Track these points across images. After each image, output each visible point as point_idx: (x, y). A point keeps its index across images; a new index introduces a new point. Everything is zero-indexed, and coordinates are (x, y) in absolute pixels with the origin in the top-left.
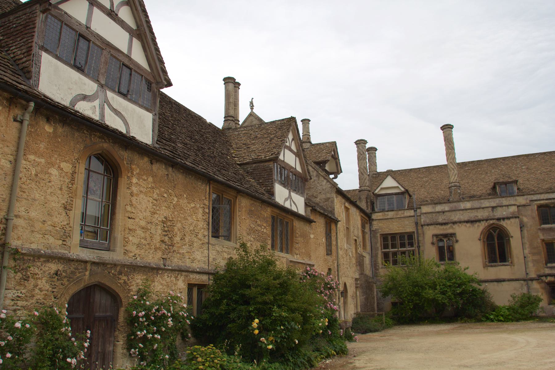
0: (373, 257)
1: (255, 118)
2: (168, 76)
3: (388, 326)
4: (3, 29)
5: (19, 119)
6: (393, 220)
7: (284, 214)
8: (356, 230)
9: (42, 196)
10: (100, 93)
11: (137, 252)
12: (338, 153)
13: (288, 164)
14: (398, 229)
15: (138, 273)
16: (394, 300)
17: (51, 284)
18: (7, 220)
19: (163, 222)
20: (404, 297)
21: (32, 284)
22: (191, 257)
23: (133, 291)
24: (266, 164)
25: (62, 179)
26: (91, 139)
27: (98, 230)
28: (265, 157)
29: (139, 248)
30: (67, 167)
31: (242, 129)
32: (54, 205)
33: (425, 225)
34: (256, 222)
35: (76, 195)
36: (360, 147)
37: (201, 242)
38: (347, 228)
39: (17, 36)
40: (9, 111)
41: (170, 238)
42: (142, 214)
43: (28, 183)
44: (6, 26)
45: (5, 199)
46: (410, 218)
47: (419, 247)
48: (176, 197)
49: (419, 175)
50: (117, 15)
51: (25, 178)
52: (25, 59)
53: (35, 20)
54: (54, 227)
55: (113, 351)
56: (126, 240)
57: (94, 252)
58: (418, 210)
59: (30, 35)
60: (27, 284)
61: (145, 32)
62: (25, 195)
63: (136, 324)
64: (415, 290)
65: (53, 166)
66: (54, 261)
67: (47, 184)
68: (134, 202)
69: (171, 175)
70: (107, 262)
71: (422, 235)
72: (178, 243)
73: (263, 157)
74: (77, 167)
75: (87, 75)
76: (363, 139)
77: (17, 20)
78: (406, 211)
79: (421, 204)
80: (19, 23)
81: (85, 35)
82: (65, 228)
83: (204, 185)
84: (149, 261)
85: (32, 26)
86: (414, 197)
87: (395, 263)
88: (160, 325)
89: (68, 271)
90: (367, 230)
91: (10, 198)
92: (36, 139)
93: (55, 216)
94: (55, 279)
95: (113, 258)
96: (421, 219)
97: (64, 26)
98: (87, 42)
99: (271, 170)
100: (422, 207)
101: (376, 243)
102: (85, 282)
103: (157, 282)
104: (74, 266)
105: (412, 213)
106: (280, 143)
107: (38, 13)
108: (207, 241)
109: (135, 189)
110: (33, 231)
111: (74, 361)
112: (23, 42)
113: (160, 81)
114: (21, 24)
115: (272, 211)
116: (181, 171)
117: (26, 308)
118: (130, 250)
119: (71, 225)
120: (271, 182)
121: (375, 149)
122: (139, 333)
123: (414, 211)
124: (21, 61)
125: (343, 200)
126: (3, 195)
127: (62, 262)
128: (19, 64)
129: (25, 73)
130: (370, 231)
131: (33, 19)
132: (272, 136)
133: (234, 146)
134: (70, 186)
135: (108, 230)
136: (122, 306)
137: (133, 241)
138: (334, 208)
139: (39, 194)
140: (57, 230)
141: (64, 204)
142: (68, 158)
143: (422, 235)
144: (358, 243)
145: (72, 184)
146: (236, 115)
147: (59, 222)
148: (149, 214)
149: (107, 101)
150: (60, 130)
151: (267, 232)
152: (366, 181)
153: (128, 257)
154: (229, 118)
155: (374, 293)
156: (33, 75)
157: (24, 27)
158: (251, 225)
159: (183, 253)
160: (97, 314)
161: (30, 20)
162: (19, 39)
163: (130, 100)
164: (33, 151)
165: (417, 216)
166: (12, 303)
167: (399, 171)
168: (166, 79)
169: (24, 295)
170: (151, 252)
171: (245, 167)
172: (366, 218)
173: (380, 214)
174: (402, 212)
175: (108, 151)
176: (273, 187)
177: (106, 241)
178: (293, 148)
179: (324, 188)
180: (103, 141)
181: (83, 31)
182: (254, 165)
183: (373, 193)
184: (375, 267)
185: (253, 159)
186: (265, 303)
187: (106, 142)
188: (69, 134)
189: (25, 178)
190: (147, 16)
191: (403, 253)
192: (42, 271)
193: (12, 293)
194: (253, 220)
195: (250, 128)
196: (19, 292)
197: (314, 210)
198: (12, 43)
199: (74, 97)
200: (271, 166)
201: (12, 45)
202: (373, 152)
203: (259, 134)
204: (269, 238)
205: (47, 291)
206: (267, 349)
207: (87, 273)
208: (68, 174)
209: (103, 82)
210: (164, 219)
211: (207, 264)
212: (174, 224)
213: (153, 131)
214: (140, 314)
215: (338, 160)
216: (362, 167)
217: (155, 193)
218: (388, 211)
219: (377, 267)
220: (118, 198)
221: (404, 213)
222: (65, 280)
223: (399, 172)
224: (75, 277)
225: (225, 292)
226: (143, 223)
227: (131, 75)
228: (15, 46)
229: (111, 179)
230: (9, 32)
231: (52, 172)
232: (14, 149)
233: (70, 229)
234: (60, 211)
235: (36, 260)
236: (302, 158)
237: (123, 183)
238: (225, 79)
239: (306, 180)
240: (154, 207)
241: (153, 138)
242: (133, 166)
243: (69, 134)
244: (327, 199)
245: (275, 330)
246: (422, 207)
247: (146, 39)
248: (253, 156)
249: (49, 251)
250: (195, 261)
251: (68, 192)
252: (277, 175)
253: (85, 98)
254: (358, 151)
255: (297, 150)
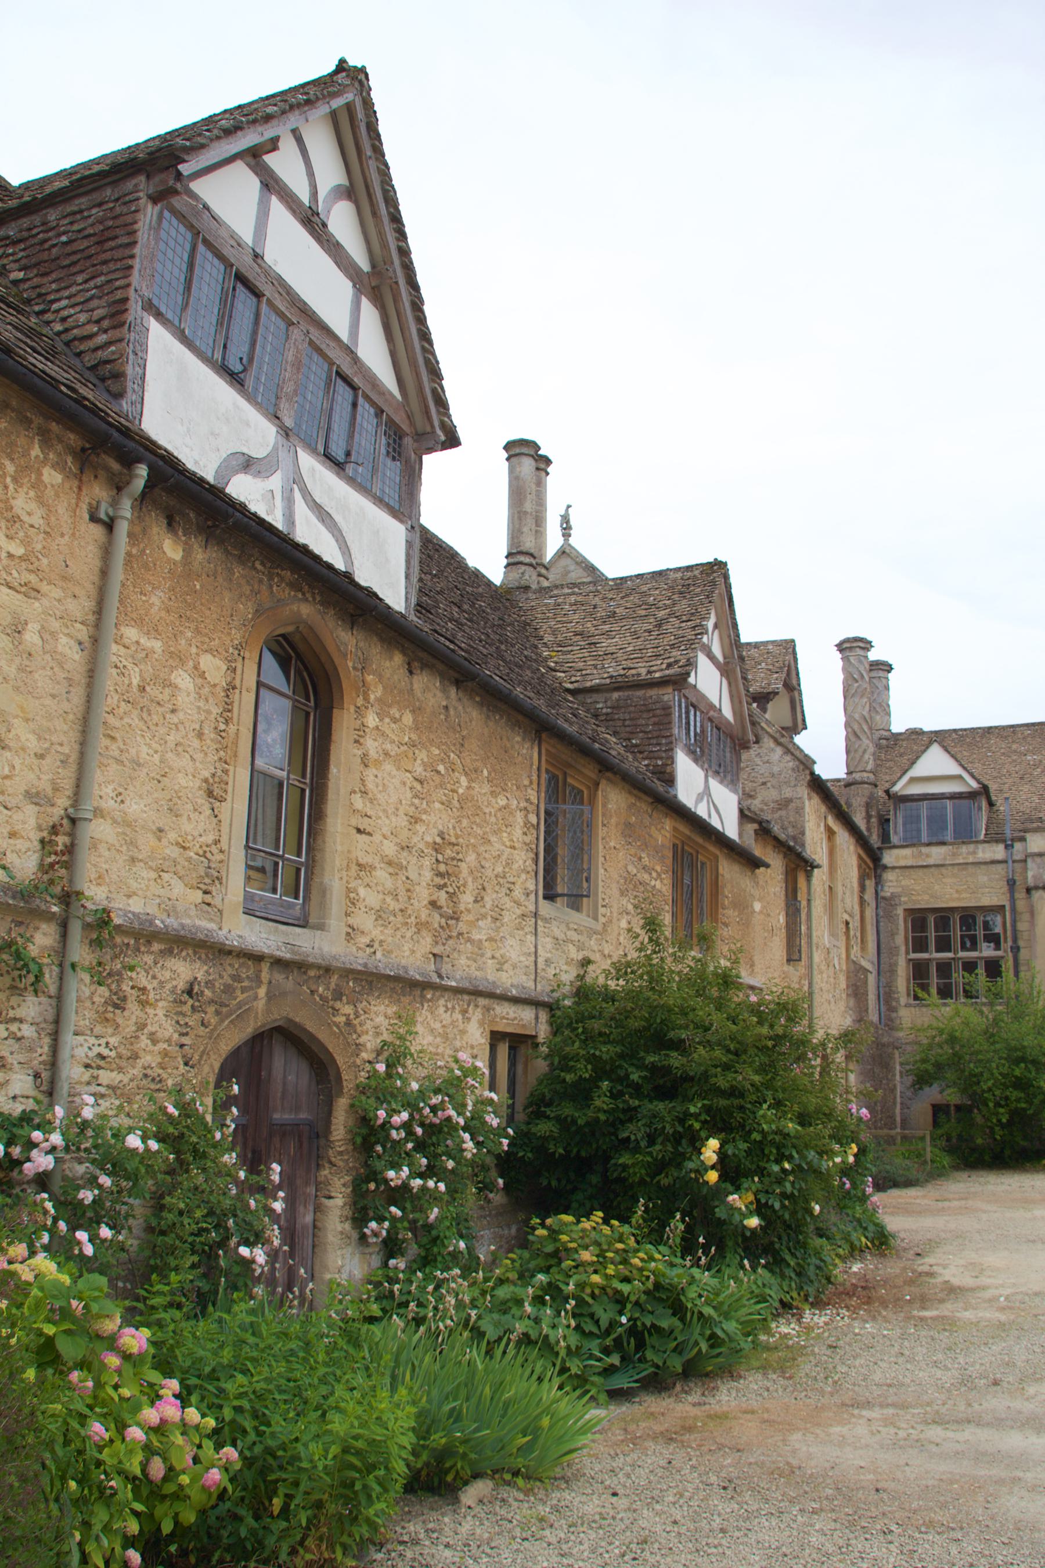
0: (885, 970)
1: (577, 563)
2: (449, 417)
3: (935, 1174)
4: (24, 250)
5: (103, 516)
6: (943, 870)
7: (700, 840)
8: (848, 894)
9: (156, 752)
10: (283, 454)
11: (376, 933)
12: (797, 674)
13: (703, 697)
14: (956, 896)
15: (378, 997)
16: (952, 1096)
17: (178, 1022)
18: (73, 821)
19: (437, 848)
20: (983, 1091)
21: (134, 1019)
22: (498, 955)
23: (366, 1051)
24: (653, 692)
25: (201, 704)
26: (271, 587)
27: (276, 864)
28: (649, 672)
29: (380, 922)
30: (214, 666)
31: (567, 591)
32: (183, 783)
33: (1037, 888)
34: (640, 859)
35: (235, 756)
36: (852, 659)
37: (519, 912)
38: (830, 888)
39: (74, 270)
40: (80, 488)
41: (451, 895)
42: (387, 822)
43: (121, 710)
44: (36, 241)
45: (68, 756)
46: (993, 867)
47: (1016, 949)
48: (466, 774)
49: (1014, 746)
50: (325, 225)
51: (116, 697)
52: (102, 338)
53: (136, 222)
54: (184, 848)
55: (315, 1227)
56: (352, 895)
57: (276, 930)
58: (1018, 846)
59: (119, 265)
60: (120, 1021)
61: (396, 283)
62: (114, 749)
63: (379, 1148)
64: (1017, 1072)
65: (182, 662)
66: (184, 954)
67: (168, 716)
68: (370, 786)
69: (455, 708)
70: (311, 959)
71: (1026, 917)
72: (468, 911)
73: (643, 671)
74: (239, 671)
75: (250, 398)
76: (851, 635)
77: (72, 223)
78: (980, 846)
79: (1022, 827)
80: (79, 231)
81: (251, 278)
82: (209, 855)
83: (527, 745)
84: (404, 962)
85: (125, 240)
86: (1001, 807)
87: (945, 992)
88: (439, 1150)
89: (217, 985)
90: (869, 896)
91: (82, 754)
92: (143, 579)
93: (185, 817)
94: (187, 1008)
95: (320, 949)
96: (1025, 869)
97: (201, 248)
98: (254, 300)
99: (667, 709)
100: (1028, 836)
101: (893, 935)
102: (256, 1017)
103: (422, 1023)
104: (230, 970)
105: (998, 852)
106: (690, 635)
107: (142, 201)
108: (532, 908)
109: (372, 745)
110: (133, 860)
111: (260, 1256)
112: (96, 287)
113: (428, 429)
114: (86, 233)
115: (675, 829)
116: (478, 699)
117: (119, 1092)
118: (361, 927)
119: (224, 845)
120: (667, 744)
121: (889, 668)
122: (391, 1174)
123: (1006, 847)
124: (91, 344)
125: (823, 809)
126: (61, 745)
127: (203, 956)
128: (82, 352)
129: (103, 380)
130: (877, 898)
131: (129, 219)
132: (661, 614)
133: (548, 638)
134: (222, 727)
135: (301, 863)
136: (340, 1093)
137: (367, 902)
138: (803, 827)
139: (149, 746)
140: (189, 860)
141: (206, 781)
142: (217, 641)
143: (1026, 917)
144: (852, 933)
145: (227, 722)
146: (540, 550)
147: (196, 834)
148: (402, 821)
149: (297, 479)
150: (200, 555)
151: (664, 889)
152: (866, 756)
153: (354, 949)
154: (522, 558)
155: (894, 1075)
156: (129, 384)
157: (98, 243)
158: (630, 868)
159: (480, 941)
160: (276, 1116)
161: (118, 222)
162: (80, 279)
163: (351, 481)
164: (134, 616)
165: (1014, 862)
166: (86, 1077)
167: (955, 731)
168: (443, 425)
169: (113, 1054)
170: (409, 934)
171: (589, 701)
172: (868, 861)
173: (907, 852)
174: (971, 847)
175: (311, 628)
176: (671, 760)
177: (297, 897)
178: (717, 650)
179: (776, 769)
180: (300, 596)
181: (244, 263)
182: (616, 695)
183: (887, 792)
184: (887, 1002)
185: (611, 677)
186: (735, 1092)
187: (307, 600)
188: (219, 569)
189: (116, 697)
190: (402, 235)
191: (970, 966)
192: (155, 982)
193: (86, 1045)
194: (633, 851)
195: (591, 588)
196: (103, 1041)
197: (764, 831)
198: (58, 291)
199: (225, 460)
200: (666, 698)
201: (58, 296)
202: (881, 674)
203: (619, 606)
204: (667, 908)
205: (168, 1041)
206: (745, 1227)
207: (262, 992)
208: (218, 689)
209: (289, 422)
210: (438, 840)
211: (533, 977)
212: (460, 856)
213: (407, 577)
214: (397, 1120)
215: (796, 693)
216: (857, 716)
217: (419, 762)
218: (929, 844)
219: (894, 1004)
220: (333, 770)
221: (974, 853)
222: (211, 1009)
223: (954, 735)
224: (235, 1002)
225: (605, 1057)
226: (389, 848)
227: (355, 405)
228: (69, 298)
229: (308, 714)
230: (45, 256)
231: (179, 681)
232: (89, 604)
233: (221, 857)
234: (199, 801)
235: (143, 949)
236: (736, 680)
237: (344, 723)
238: (509, 446)
239: (745, 746)
240: (416, 801)
241: (407, 599)
242: (370, 678)
243: (219, 569)
244: (784, 804)
245: (762, 1172)
246: (1028, 836)
247: (395, 301)
248: (612, 669)
249: (172, 922)
250: (505, 967)
251: (219, 746)
252: (680, 727)
253: (248, 464)
254: (844, 669)
255: (725, 658)
